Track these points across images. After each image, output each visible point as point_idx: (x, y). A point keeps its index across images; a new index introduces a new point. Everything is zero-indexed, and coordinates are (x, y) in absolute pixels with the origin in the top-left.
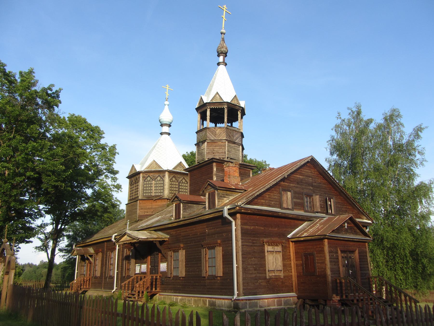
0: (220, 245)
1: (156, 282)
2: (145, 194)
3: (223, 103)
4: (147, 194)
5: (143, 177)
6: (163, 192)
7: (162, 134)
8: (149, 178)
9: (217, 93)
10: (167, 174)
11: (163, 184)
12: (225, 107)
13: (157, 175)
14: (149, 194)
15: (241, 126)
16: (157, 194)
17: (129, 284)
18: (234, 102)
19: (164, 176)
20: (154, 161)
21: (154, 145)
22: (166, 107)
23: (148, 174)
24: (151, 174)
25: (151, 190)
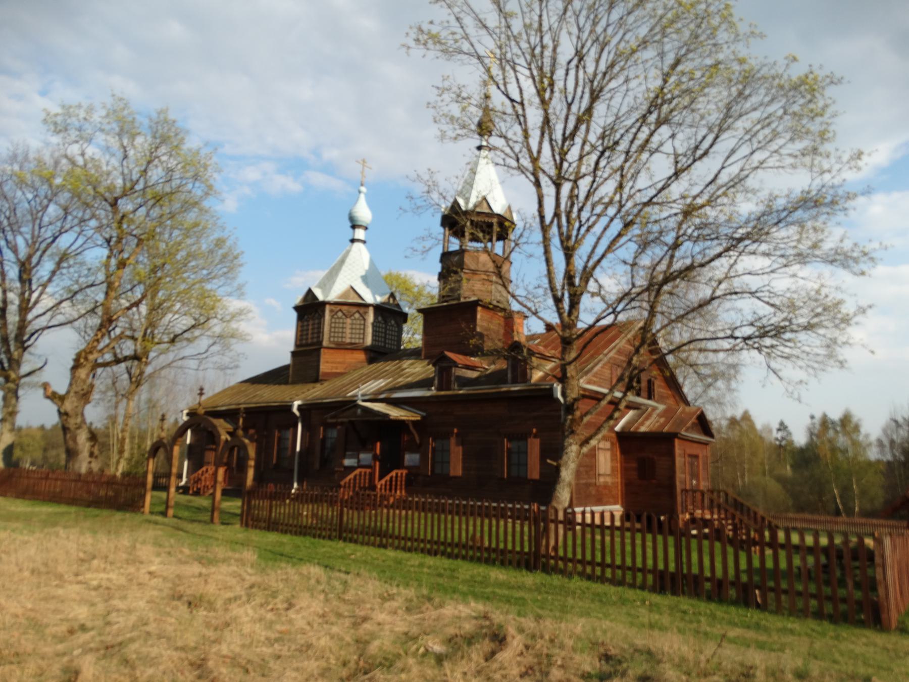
0: (536, 436)
1: (396, 481)
2: (332, 339)
3: (492, 215)
4: (336, 339)
5: (331, 311)
6: (363, 339)
7: (353, 241)
8: (340, 314)
9: (485, 199)
10: (371, 312)
11: (364, 325)
12: (495, 220)
13: (354, 309)
14: (340, 340)
15: (446, 241)
16: (353, 341)
17: (386, 485)
18: (507, 216)
19: (366, 313)
20: (352, 288)
21: (339, 258)
22: (362, 196)
23: (339, 307)
24: (344, 308)
25: (342, 333)
